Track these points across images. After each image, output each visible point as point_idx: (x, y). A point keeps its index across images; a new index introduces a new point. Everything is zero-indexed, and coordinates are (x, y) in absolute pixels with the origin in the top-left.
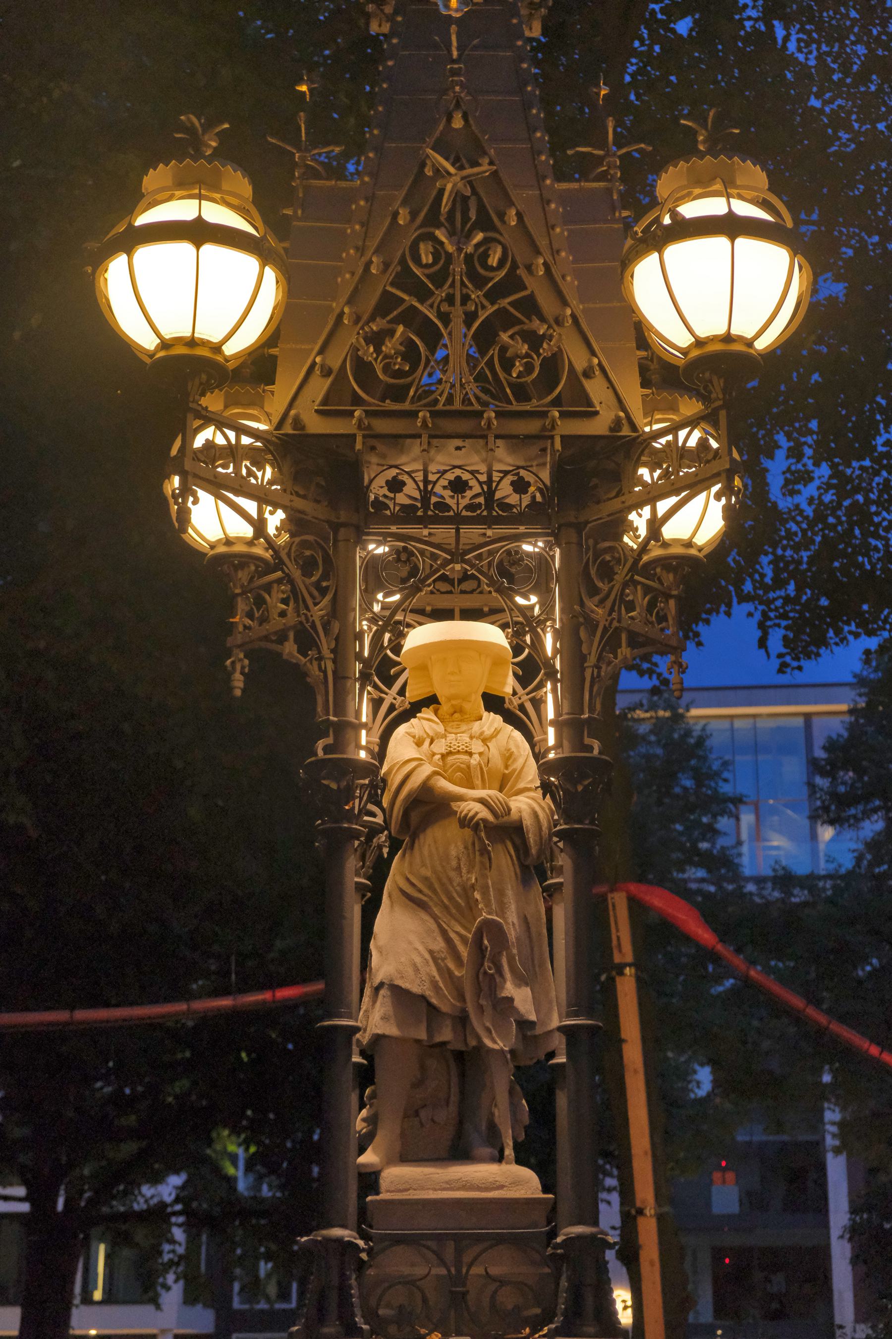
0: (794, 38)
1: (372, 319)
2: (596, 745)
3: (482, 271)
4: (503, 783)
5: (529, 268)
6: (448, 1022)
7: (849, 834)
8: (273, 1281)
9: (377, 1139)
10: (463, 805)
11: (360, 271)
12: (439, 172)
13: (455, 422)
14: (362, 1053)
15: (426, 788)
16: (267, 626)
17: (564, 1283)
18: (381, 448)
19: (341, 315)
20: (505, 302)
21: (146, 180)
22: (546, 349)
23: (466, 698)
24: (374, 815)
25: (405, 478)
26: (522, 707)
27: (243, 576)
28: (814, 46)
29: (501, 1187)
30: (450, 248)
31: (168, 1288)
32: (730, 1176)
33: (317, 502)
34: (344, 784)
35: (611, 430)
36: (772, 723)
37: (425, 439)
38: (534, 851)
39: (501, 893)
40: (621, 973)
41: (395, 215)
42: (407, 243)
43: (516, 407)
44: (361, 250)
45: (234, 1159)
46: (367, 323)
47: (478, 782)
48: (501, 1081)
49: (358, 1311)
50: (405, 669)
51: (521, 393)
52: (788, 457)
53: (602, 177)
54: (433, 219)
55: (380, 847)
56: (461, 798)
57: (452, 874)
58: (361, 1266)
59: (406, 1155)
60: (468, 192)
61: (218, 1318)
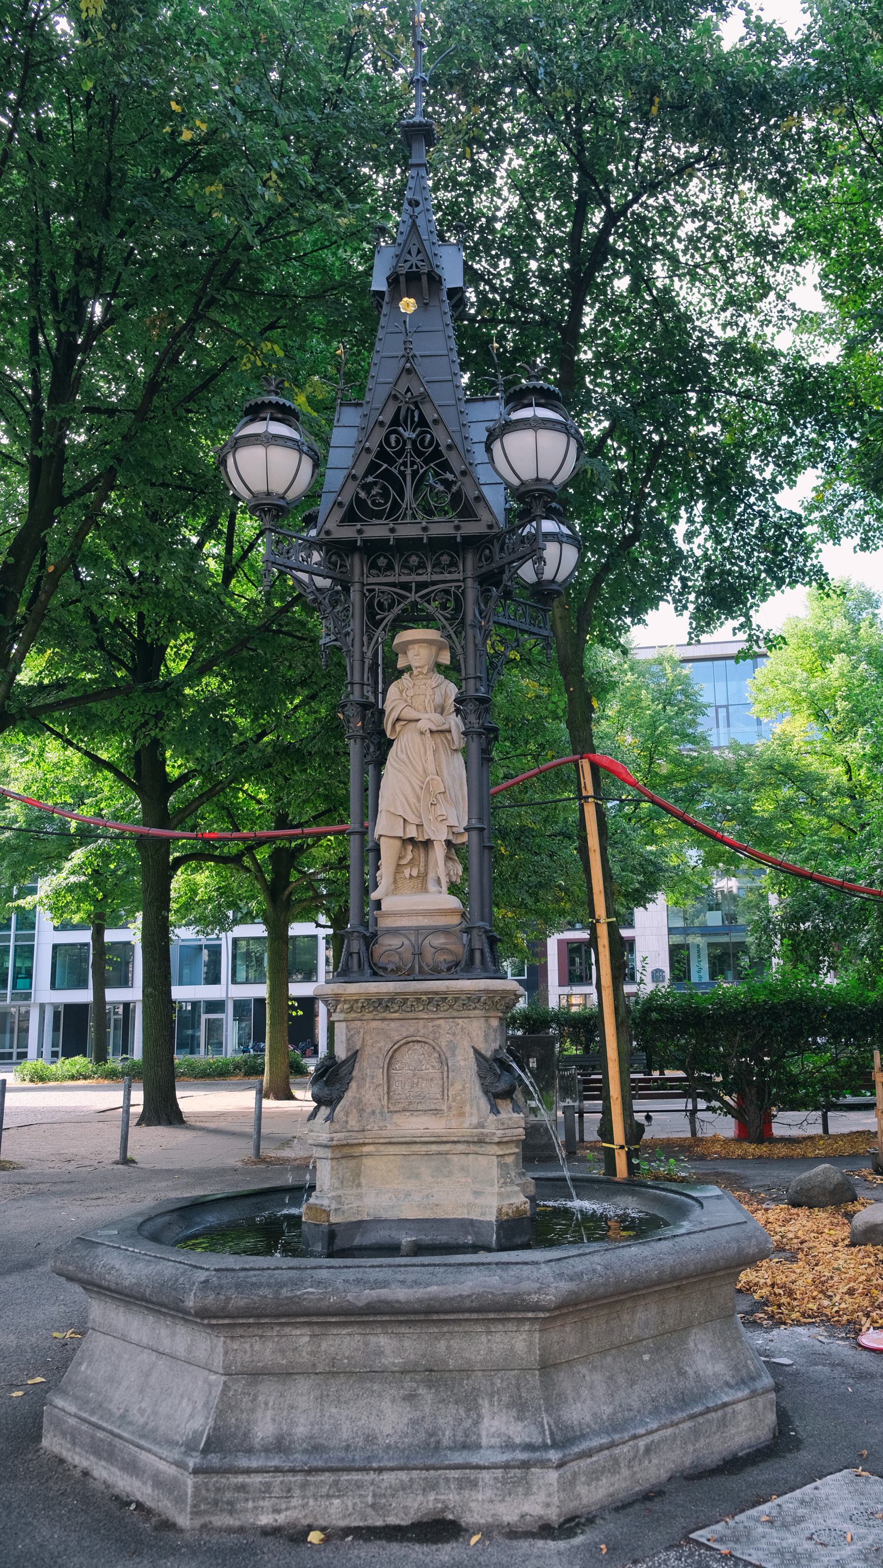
22: (454, 489)
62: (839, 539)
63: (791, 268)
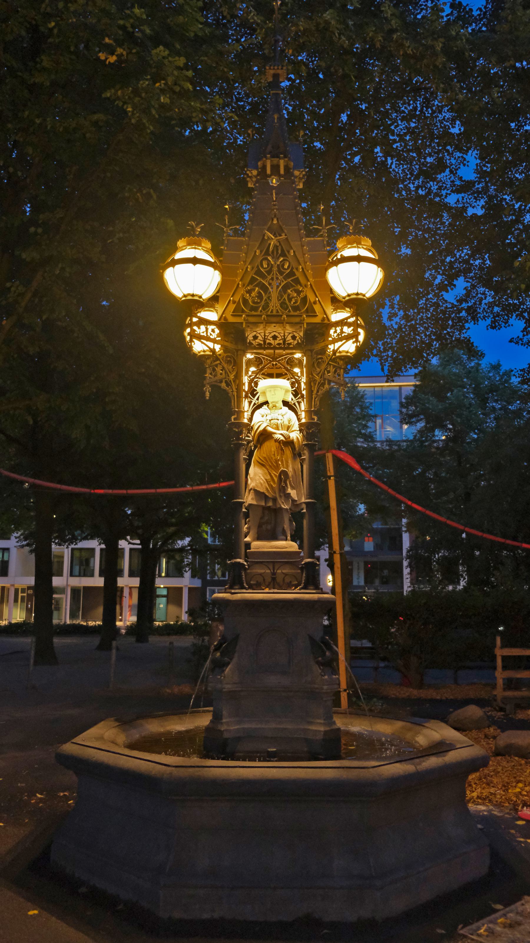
0: (394, 163)
1: (248, 285)
2: (316, 418)
3: (282, 270)
4: (288, 428)
5: (297, 269)
6: (271, 500)
7: (413, 427)
8: (220, 571)
9: (250, 534)
10: (276, 435)
11: (244, 270)
12: (269, 238)
13: (274, 319)
14: (246, 509)
15: (265, 430)
16: (216, 378)
17: (304, 575)
18: (251, 326)
19: (239, 284)
20: (289, 280)
21: (178, 243)
23: (277, 402)
24: (249, 437)
25: (258, 335)
26: (294, 404)
27: (209, 361)
28: (401, 166)
29: (286, 548)
30: (273, 263)
31: (186, 572)
32: (371, 539)
33: (231, 343)
34: (240, 430)
35: (322, 321)
36: (388, 389)
37: (264, 323)
38: (297, 449)
39: (287, 462)
40: (330, 479)
41: (256, 252)
42: (259, 261)
43: (292, 313)
44: (245, 262)
45: (207, 533)
46: (246, 287)
47: (280, 428)
48: (286, 518)
49: (245, 582)
50: (258, 393)
51: (296, 309)
52: (389, 308)
53: (321, 236)
54: (267, 253)
55: (251, 447)
56: (275, 433)
57: (273, 456)
58: (246, 569)
59: (259, 538)
60: (278, 244)
61: (202, 582)
62: (478, 321)
63: (461, 155)
